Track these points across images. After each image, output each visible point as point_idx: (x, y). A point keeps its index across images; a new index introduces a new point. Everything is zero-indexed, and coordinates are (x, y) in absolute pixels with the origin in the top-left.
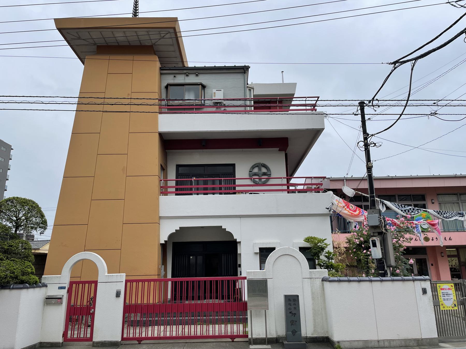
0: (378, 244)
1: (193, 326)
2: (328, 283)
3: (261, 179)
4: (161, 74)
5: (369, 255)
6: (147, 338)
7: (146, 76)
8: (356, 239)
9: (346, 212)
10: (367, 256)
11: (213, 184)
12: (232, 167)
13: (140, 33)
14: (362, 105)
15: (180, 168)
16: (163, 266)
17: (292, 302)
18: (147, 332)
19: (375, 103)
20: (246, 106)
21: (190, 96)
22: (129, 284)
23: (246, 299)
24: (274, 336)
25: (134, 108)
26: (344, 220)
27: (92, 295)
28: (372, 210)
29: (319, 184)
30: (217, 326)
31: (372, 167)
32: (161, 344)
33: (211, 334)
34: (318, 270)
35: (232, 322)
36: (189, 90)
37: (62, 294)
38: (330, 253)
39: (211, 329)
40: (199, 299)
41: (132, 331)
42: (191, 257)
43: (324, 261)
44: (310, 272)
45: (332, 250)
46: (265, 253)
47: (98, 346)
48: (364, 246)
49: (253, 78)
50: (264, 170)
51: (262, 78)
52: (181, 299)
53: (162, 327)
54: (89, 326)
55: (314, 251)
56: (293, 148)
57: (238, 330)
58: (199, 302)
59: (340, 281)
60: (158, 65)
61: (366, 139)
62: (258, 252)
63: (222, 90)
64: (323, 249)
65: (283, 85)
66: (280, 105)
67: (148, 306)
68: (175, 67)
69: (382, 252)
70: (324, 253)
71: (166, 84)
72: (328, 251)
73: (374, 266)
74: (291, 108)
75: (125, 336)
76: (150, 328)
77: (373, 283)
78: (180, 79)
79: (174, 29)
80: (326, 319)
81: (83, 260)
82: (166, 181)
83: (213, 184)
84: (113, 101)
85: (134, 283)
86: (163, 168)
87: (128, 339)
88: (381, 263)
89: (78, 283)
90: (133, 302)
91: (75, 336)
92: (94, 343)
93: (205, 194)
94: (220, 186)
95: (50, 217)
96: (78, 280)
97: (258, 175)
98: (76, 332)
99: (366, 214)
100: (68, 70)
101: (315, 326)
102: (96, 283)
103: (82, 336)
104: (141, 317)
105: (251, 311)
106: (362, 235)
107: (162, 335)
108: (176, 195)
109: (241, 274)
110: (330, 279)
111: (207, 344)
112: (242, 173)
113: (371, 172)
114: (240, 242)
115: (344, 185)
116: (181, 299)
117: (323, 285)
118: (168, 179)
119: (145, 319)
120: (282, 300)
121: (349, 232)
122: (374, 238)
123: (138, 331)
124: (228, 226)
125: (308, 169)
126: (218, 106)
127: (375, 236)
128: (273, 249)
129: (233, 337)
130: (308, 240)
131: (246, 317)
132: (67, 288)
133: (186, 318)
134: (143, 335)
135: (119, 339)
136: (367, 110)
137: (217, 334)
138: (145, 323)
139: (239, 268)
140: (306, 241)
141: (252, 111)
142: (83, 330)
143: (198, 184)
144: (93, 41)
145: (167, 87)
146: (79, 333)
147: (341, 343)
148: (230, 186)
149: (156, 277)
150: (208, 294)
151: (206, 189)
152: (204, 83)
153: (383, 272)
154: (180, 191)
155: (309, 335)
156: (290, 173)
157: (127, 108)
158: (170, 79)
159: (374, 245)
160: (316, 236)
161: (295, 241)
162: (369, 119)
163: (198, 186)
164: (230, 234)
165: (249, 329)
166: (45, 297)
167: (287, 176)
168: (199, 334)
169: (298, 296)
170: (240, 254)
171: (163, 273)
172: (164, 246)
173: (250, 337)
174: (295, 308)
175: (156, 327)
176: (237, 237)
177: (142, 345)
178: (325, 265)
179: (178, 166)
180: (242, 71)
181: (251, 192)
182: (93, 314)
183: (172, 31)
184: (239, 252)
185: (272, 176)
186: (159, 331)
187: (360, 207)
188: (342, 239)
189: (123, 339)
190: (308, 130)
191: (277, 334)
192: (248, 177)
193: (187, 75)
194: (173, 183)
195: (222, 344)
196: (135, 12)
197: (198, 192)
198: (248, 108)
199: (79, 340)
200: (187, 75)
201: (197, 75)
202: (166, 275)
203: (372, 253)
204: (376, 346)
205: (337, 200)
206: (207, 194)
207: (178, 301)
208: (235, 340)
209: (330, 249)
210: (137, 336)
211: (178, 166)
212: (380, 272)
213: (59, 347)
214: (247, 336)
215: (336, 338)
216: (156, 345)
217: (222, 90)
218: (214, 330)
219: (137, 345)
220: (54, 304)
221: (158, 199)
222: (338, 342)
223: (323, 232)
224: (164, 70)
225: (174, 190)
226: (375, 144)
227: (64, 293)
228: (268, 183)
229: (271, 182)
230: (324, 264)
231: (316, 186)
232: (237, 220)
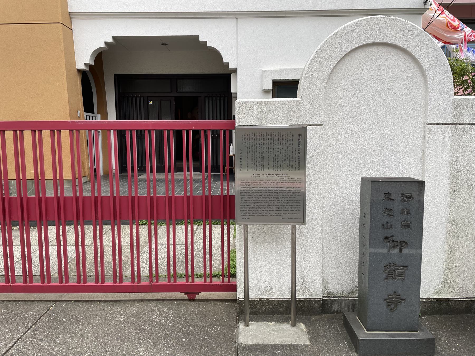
42: (151, 103)
44: (457, 105)
90: (52, 231)
101: (448, 271)
114: (235, 71)
120: (353, 194)
124: (213, 35)
164: (215, 55)
173: (240, 294)
174: (406, 225)
176: (229, 58)
184: (233, 91)
191: (324, 282)
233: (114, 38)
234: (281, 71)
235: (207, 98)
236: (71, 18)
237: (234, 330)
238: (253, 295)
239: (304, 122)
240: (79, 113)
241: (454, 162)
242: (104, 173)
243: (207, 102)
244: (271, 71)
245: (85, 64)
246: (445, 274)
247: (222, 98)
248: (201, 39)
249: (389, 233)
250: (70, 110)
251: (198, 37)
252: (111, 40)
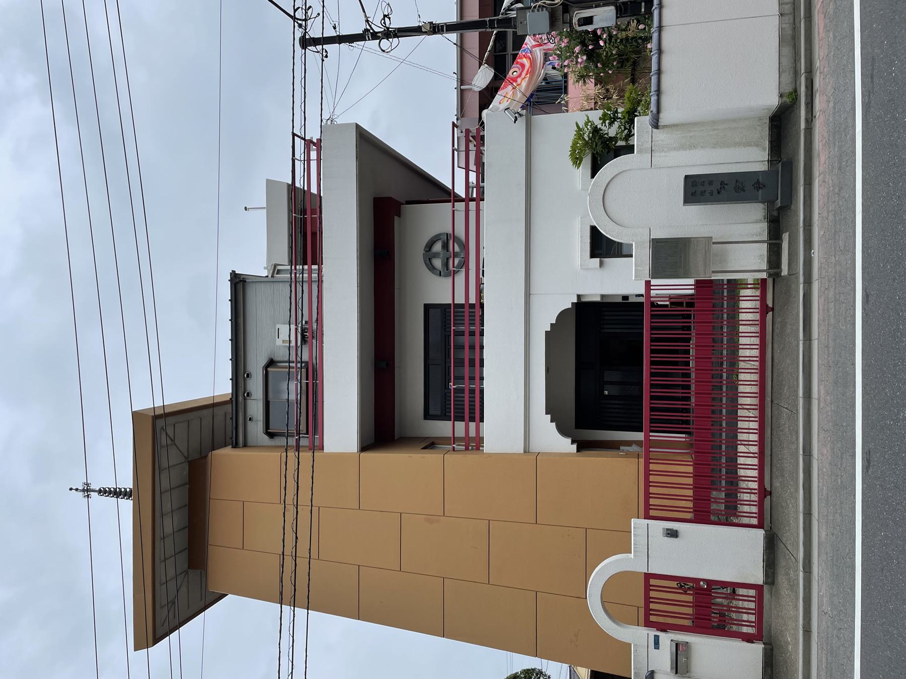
0: (586, 13)
1: (741, 389)
2: (662, 115)
3: (454, 254)
4: (245, 445)
5: (610, 36)
6: (761, 479)
7: (248, 476)
8: (577, 62)
9: (524, 84)
10: (610, 40)
11: (463, 347)
12: (431, 311)
13: (165, 484)
14: (306, 42)
15: (432, 412)
16: (622, 448)
17: (699, 189)
18: (748, 479)
19: (299, 14)
20: (310, 281)
21: (292, 390)
22: (652, 513)
23: (691, 281)
24: (764, 226)
25: (304, 497)
26: (539, 90)
27: (674, 584)
28: (518, 24)
29: (467, 136)
30: (742, 341)
31: (431, 23)
32: (774, 450)
33: (756, 353)
34: (635, 141)
35: (734, 310)
36: (278, 392)
37: (669, 642)
38: (605, 115)
39: (748, 353)
40: (688, 375)
41: (746, 508)
43: (619, 127)
44: (640, 152)
45: (600, 113)
46: (602, 247)
47: (774, 573)
48: (588, 42)
49: (256, 265)
50: (438, 247)
51: (256, 248)
52: (687, 411)
53: (741, 448)
54: (734, 591)
55: (599, 149)
56: (394, 189)
57: (751, 299)
58: (693, 375)
59: (659, 92)
60: (228, 451)
61: (375, 36)
62: (598, 259)
63: (278, 326)
64: (596, 130)
65: (270, 208)
66: (309, 212)
67: (696, 476)
68: (232, 418)
69: (604, 5)
70: (603, 128)
71: (266, 437)
72: (600, 119)
73: (634, 24)
74: (314, 190)
75: (754, 521)
76: (741, 472)
77: (664, 23)
78: (256, 408)
79: (156, 418)
80: (734, 120)
81: (603, 602)
82: (455, 439)
83: (462, 347)
84: (290, 536)
85: (652, 501)
86: (431, 444)
87: (761, 515)
88: (626, 10)
89: (648, 612)
91: (752, 618)
92: (766, 583)
93: (482, 365)
94: (467, 334)
95: (523, 662)
96: (642, 611)
97: (448, 259)
98: (745, 617)
99: (529, 41)
100: (234, 624)
101: (748, 144)
102: (648, 576)
103: (752, 605)
104: (720, 490)
105: (713, 272)
106: (570, 49)
107: (755, 449)
108: (482, 420)
109: (642, 295)
110: (655, 111)
111: (776, 360)
112: (442, 291)
113: (442, 26)
114: (579, 296)
115: (471, 89)
116: (696, 452)
117: (665, 126)
118: (451, 435)
119: (723, 483)
120: (694, 210)
121: (566, 82)
122: (575, 20)
123: (746, 497)
125: (437, 159)
126: (310, 334)
127: (571, 20)
128: (594, 229)
129: (764, 310)
130: (577, 161)
131: (725, 282)
132: (658, 633)
133: (725, 352)
134: (755, 485)
135: (761, 533)
136: (315, 32)
137: (757, 341)
138: (732, 482)
139: (631, 300)
140: (580, 164)
141: (320, 270)
142: (740, 604)
143: (463, 378)
144: (179, 574)
145: (272, 435)
146: (748, 611)
147: (782, 90)
148: (467, 314)
149: (642, 460)
150: (679, 358)
151: (472, 363)
152: (263, 362)
153: (643, 4)
154: (476, 414)
155: (764, 155)
156: (444, 194)
157: (304, 513)
158: (256, 429)
159: (589, 21)
160: (571, 144)
161: (579, 186)
162: (335, 28)
163: (467, 378)
164: (562, 315)
165: (750, 278)
166: (673, 674)
167: (450, 201)
168: (755, 377)
169: (687, 177)
170: (602, 296)
171: (634, 448)
172: (583, 446)
173: (764, 275)
174: (711, 183)
175: (741, 460)
176: (567, 302)
177: (773, 488)
178: (627, 126)
179: (427, 416)
180: (240, 286)
181: (480, 273)
182: (710, 582)
183: (160, 423)
184: (598, 299)
185: (450, 231)
186: (748, 455)
187: (515, 57)
188: (580, 92)
189: (760, 526)
190: (359, 157)
191: (760, 221)
192: (450, 280)
193: (248, 395)
194: (460, 426)
195: (776, 331)
196: (125, 495)
197: (477, 378)
198: (315, 276)
199: (759, 612)
200: (248, 395)
201: (248, 376)
202: (638, 443)
203: (605, 25)
204: (792, 21)
205: (499, 102)
206: (482, 361)
207: (692, 417)
208: (770, 304)
209: (596, 116)
210: (754, 497)
211: (427, 416)
212: (643, 10)
213: (772, 650)
214: (764, 281)
215: (773, 101)
216: (774, 461)
217: (278, 326)
218: (750, 347)
219: (774, 499)
220: (688, 657)
221: (490, 455)
222: (781, 96)
223: (561, 129)
224: (236, 439)
225: (472, 425)
226: (385, 16)
227: (666, 639)
228: (463, 238)
229: (460, 232)
230: (625, 129)
231: (472, 142)
232: (534, 300)
237: (785, 276)
238: (764, 266)
239: (647, 239)
241: (675, 149)
246: (751, 146)
249: (715, 192)
252: (549, 416)
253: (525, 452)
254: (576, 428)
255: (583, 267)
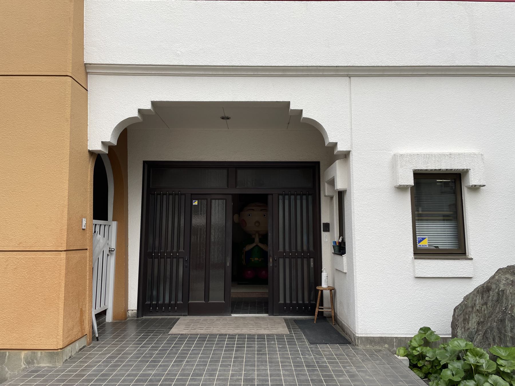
114: (346, 155)
117: (414, 267)
124: (309, 101)
164: (313, 131)
176: (335, 134)
226: (97, 339)
233: (153, 103)
234: (428, 157)
235: (281, 197)
236: (87, 73)
240: (84, 222)
242: (114, 317)
243: (299, 202)
244: (411, 155)
245: (102, 142)
247: (304, 197)
248: (292, 107)
250: (69, 219)
251: (288, 103)
252: (149, 107)
253: (85, 64)
254: (144, 162)
255: (395, 161)
